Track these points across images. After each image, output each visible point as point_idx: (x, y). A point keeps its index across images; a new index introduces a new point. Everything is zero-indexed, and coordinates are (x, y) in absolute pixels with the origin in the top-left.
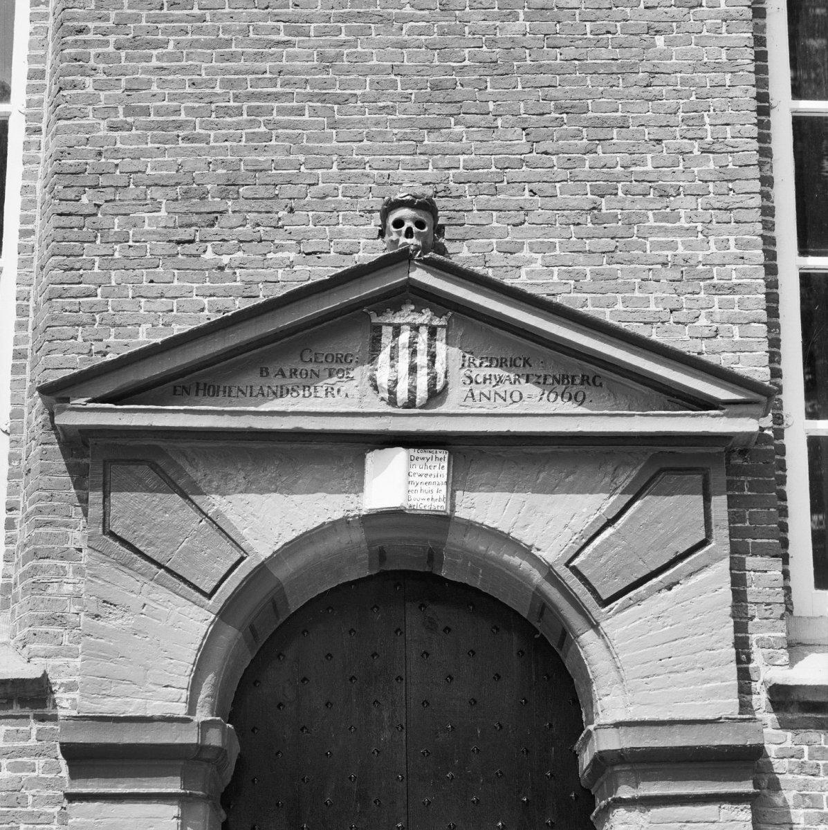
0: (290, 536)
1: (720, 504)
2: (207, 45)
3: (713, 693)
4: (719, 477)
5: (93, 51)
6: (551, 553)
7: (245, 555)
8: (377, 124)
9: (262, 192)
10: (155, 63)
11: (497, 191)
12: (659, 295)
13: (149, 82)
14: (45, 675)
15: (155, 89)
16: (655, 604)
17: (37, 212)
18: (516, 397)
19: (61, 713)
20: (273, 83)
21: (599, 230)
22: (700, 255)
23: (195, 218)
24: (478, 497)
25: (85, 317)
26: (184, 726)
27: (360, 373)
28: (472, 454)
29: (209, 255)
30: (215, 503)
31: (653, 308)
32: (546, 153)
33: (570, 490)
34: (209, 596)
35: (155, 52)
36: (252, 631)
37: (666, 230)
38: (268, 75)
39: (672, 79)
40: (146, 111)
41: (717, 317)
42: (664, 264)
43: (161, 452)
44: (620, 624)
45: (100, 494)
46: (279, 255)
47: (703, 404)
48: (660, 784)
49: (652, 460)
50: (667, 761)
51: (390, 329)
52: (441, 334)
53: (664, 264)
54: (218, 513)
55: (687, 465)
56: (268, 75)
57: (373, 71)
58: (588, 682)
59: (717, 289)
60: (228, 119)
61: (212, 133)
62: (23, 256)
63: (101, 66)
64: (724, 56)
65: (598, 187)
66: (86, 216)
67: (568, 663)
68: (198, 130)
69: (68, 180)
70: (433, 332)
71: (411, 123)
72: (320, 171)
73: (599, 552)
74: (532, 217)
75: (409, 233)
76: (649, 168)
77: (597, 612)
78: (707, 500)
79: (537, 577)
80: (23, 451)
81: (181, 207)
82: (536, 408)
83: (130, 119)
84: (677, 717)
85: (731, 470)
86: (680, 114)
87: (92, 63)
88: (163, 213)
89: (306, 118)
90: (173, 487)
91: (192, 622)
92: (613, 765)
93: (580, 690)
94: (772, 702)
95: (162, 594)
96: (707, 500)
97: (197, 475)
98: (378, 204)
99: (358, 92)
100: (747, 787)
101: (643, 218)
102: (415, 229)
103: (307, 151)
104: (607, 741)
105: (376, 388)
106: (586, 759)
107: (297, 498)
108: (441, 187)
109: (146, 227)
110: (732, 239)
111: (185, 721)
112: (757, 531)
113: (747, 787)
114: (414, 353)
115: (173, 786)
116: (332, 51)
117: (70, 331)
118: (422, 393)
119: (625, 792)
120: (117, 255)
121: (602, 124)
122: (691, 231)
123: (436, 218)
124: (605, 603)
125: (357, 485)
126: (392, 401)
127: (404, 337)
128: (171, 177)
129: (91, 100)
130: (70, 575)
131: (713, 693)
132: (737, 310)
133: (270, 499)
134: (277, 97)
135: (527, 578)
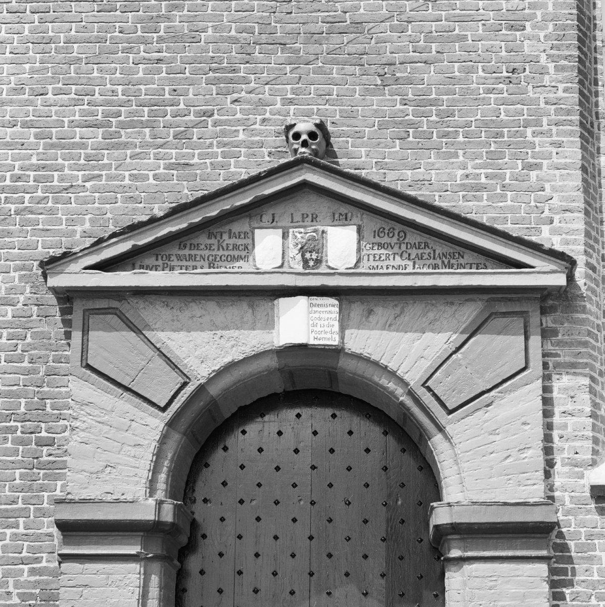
6: (414, 378)
7: (188, 380)
24: (363, 333)
44: (454, 426)
78: (527, 339)
91: (154, 425)
92: (447, 535)
96: (527, 339)
115: (142, 534)
119: (455, 553)
124: (450, 412)
125: (269, 324)
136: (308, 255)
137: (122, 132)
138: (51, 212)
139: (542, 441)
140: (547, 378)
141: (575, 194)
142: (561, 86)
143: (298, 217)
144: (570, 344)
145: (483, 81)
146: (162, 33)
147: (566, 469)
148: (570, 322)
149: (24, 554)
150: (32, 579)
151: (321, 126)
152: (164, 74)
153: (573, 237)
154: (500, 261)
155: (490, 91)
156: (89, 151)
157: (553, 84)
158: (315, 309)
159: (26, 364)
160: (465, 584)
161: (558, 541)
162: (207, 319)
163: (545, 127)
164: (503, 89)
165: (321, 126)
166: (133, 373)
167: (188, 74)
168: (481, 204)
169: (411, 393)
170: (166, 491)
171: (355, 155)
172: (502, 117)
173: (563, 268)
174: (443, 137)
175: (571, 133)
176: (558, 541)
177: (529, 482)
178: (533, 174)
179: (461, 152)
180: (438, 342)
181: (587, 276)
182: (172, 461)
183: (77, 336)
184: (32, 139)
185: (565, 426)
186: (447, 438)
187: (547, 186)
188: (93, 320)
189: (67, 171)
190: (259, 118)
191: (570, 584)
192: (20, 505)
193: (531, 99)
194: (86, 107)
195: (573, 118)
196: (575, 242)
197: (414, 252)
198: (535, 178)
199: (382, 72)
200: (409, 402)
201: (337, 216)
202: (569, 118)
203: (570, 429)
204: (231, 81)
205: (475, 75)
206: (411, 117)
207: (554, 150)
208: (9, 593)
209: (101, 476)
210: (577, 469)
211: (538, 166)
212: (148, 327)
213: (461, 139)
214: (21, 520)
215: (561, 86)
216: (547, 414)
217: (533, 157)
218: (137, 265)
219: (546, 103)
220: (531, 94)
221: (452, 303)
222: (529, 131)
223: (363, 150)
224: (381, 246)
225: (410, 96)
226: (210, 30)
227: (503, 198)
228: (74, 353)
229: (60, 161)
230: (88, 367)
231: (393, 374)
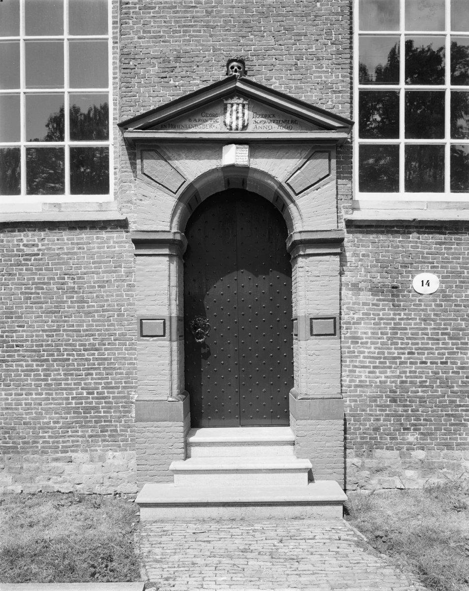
0: (200, 174)
1: (334, 161)
2: (169, 8)
3: (330, 222)
4: (334, 153)
5: (131, 11)
6: (281, 179)
8: (225, 35)
9: (188, 60)
10: (152, 15)
11: (264, 59)
12: (316, 94)
13: (150, 21)
14: (127, 218)
15: (152, 24)
16: (312, 194)
17: (118, 71)
18: (270, 127)
19: (131, 230)
20: (190, 21)
21: (297, 72)
22: (330, 80)
23: (167, 69)
25: (133, 104)
26: (168, 233)
27: (220, 119)
28: (256, 146)
29: (172, 82)
30: (176, 163)
31: (314, 98)
32: (280, 45)
33: (287, 158)
34: (175, 193)
35: (152, 11)
36: (189, 206)
37: (319, 72)
38: (189, 18)
39: (322, 18)
40: (149, 32)
41: (334, 102)
42: (318, 83)
43: (158, 147)
44: (300, 200)
45: (140, 160)
46: (195, 81)
47: (329, 128)
48: (313, 249)
49: (313, 148)
50: (315, 243)
51: (230, 105)
52: (246, 106)
53: (318, 83)
54: (177, 167)
55: (323, 150)
56: (189, 18)
57: (224, 16)
58: (291, 220)
59: (335, 92)
60: (177, 34)
61: (171, 39)
62: (114, 86)
63: (134, 16)
64: (339, 10)
65: (297, 57)
66: (132, 69)
67: (284, 216)
68: (167, 38)
69: (126, 57)
70: (244, 106)
71: (236, 35)
72: (207, 52)
73: (296, 179)
74: (276, 68)
75: (236, 71)
76: (314, 50)
77: (294, 197)
78: (330, 161)
79: (276, 187)
80: (118, 150)
81: (162, 65)
82: (274, 130)
83: (145, 35)
84: (319, 229)
85: (338, 153)
86: (325, 31)
87: (131, 15)
88: (157, 68)
89: (202, 33)
91: (171, 201)
93: (288, 223)
94: (346, 225)
95: (160, 193)
96: (330, 161)
97: (170, 155)
98: (225, 63)
99: (219, 24)
100: (338, 250)
101: (311, 68)
102: (238, 70)
103: (203, 45)
104: (297, 237)
105: (225, 125)
106: (289, 244)
107: (201, 161)
108: (246, 57)
109: (152, 73)
110: (340, 74)
111: (169, 232)
112: (344, 172)
113: (338, 250)
114: (238, 112)
115: (166, 251)
116: (210, 9)
117: (128, 108)
118: (240, 126)
119: (301, 253)
120: (142, 82)
121: (299, 35)
122: (327, 72)
123: (245, 67)
125: (220, 156)
126: (231, 129)
127: (235, 107)
128: (158, 55)
129: (132, 28)
130: (133, 188)
131: (330, 222)
132: (341, 99)
134: (192, 26)
135: (273, 187)
139: (344, 274)
186: (296, 205)
218: (181, 127)
230: (144, 174)
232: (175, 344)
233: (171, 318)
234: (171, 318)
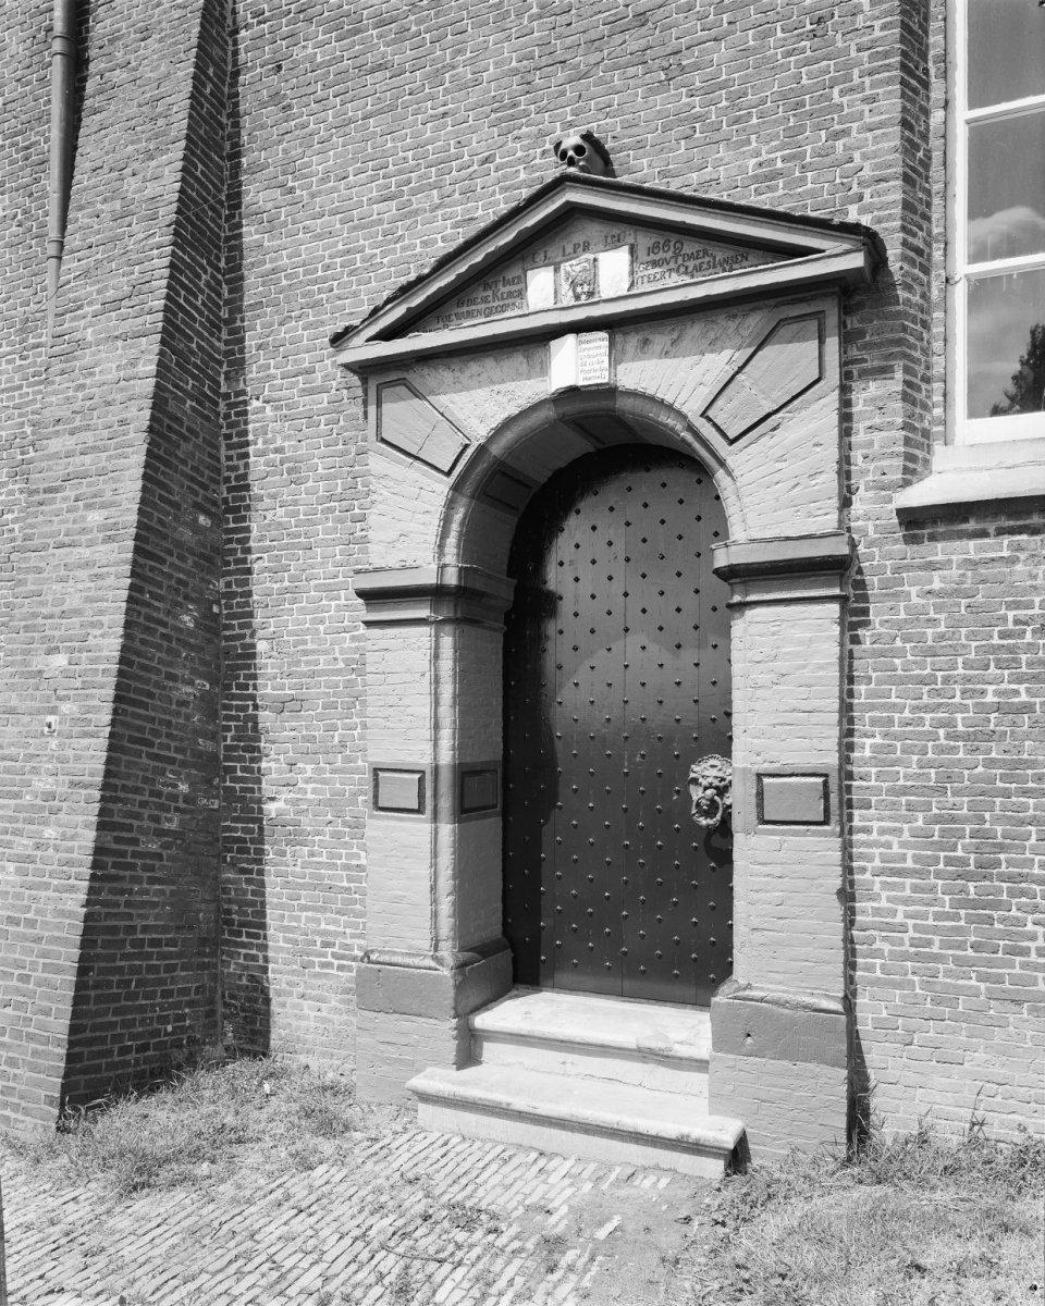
1: (832, 343)
6: (692, 408)
30: (442, 400)
34: (448, 474)
78: (821, 342)
90: (418, 395)
96: (821, 342)
100: (837, 591)
115: (424, 612)
124: (732, 442)
125: (544, 370)
133: (644, 385)
136: (579, 289)
137: (413, 199)
138: (355, 294)
140: (845, 389)
141: (891, 157)
142: (877, 24)
143: (569, 249)
144: (879, 345)
145: (781, 43)
146: (447, 85)
147: (871, 494)
148: (880, 318)
149: (346, 623)
150: (353, 645)
151: (587, 137)
152: (449, 128)
153: (888, 212)
154: (779, 252)
155: (790, 54)
156: (385, 226)
157: (868, 23)
158: (584, 346)
159: (340, 447)
160: (745, 631)
161: (859, 577)
162: (485, 376)
163: (856, 80)
164: (805, 47)
165: (587, 137)
166: (420, 442)
167: (471, 122)
168: (776, 194)
169: (691, 428)
170: (458, 555)
171: (638, 168)
172: (804, 82)
173: (860, 244)
174: (735, 123)
175: (888, 82)
176: (859, 577)
177: (820, 512)
178: (840, 144)
179: (753, 137)
180: (718, 363)
181: (904, 258)
182: (462, 524)
183: (372, 409)
184: (338, 226)
185: (871, 444)
186: (729, 474)
187: (857, 155)
188: (386, 393)
189: (367, 251)
190: (539, 151)
191: (866, 624)
192: (341, 579)
193: (840, 51)
194: (381, 181)
195: (892, 60)
196: (890, 218)
197: (691, 264)
198: (842, 148)
199: (666, 65)
200: (689, 437)
201: (609, 240)
202: (887, 62)
203: (876, 447)
204: (513, 118)
205: (772, 39)
206: (698, 109)
207: (867, 108)
208: (335, 659)
209: (397, 544)
210: (883, 493)
211: (845, 133)
212: (433, 393)
213: (755, 121)
214: (342, 592)
215: (877, 24)
216: (845, 431)
217: (840, 123)
219: (859, 50)
220: (840, 44)
221: (735, 316)
222: (836, 91)
223: (645, 161)
224: (655, 264)
225: (698, 84)
226: (491, 68)
227: (803, 180)
228: (371, 431)
229: (362, 242)
230: (383, 441)
231: (670, 407)
232: (447, 830)
233: (436, 769)
234: (436, 769)
